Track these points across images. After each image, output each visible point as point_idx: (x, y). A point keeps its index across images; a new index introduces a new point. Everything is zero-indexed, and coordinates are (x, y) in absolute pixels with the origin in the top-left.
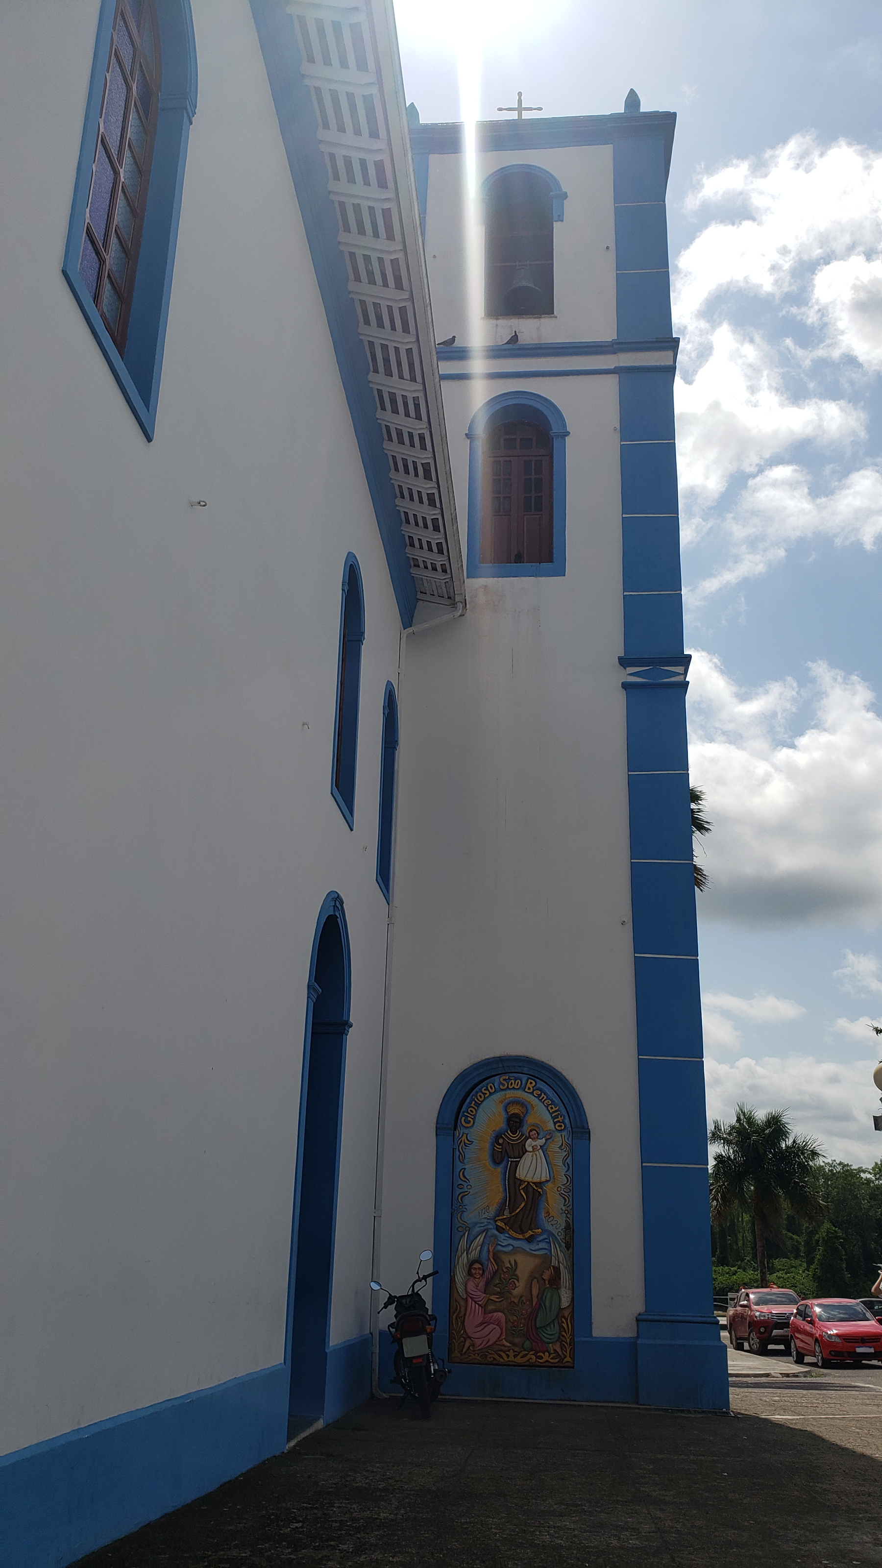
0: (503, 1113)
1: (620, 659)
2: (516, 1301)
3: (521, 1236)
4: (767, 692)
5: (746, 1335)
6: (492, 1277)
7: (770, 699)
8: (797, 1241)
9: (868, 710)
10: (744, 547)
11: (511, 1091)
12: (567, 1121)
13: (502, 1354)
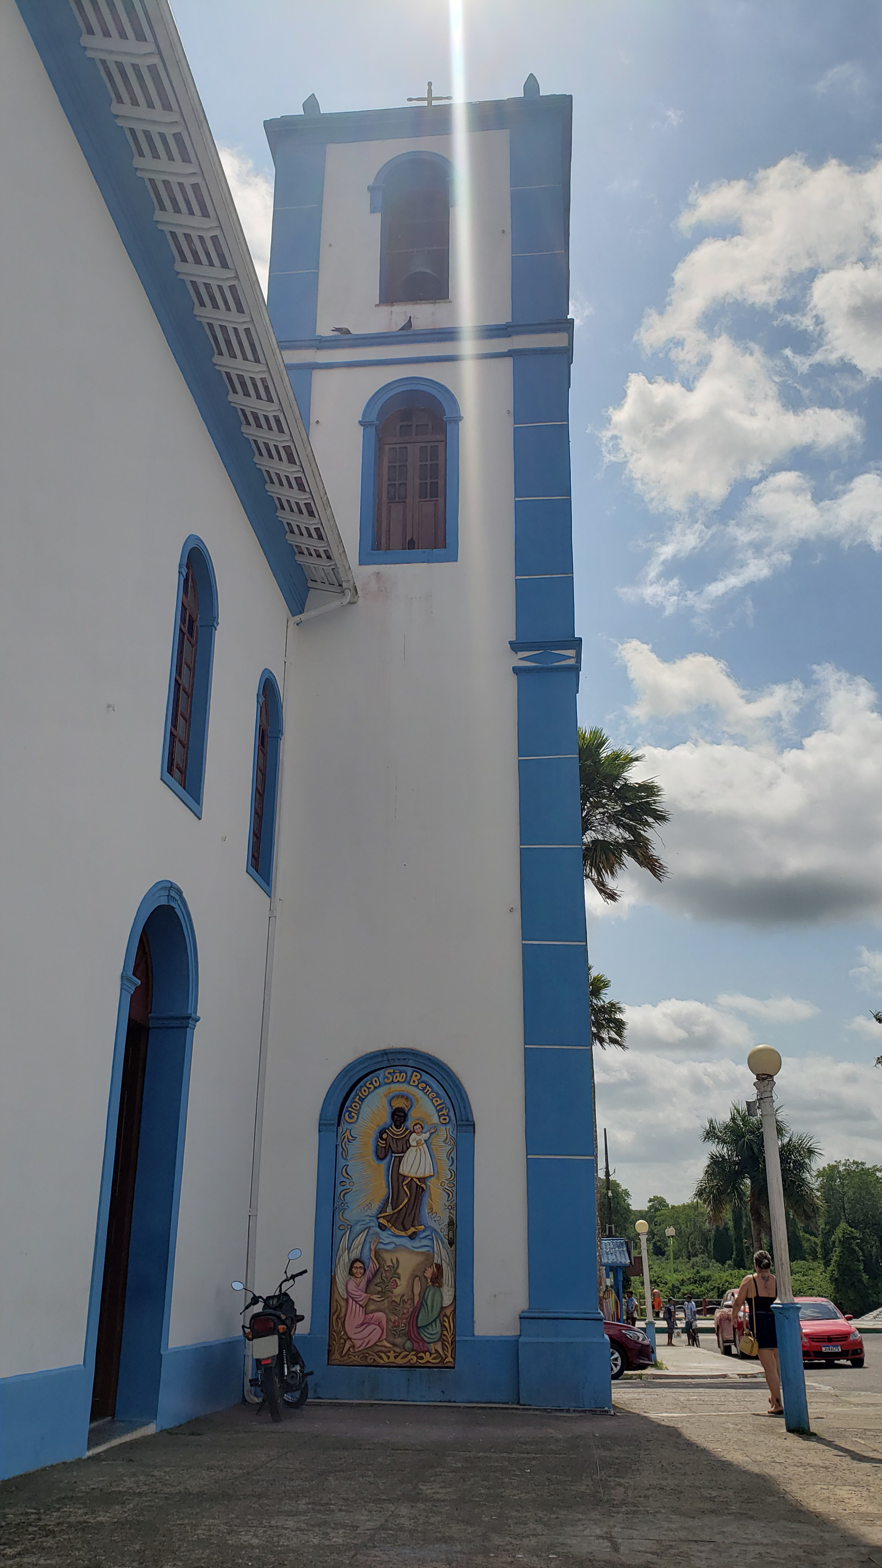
0: (388, 1107)
1: (511, 643)
2: (398, 1300)
3: (403, 1234)
4: (771, 694)
5: (731, 1337)
6: (374, 1276)
7: (778, 700)
8: (815, 1243)
9: (873, 711)
10: (750, 553)
11: (396, 1085)
12: (452, 1114)
13: (382, 1355)
